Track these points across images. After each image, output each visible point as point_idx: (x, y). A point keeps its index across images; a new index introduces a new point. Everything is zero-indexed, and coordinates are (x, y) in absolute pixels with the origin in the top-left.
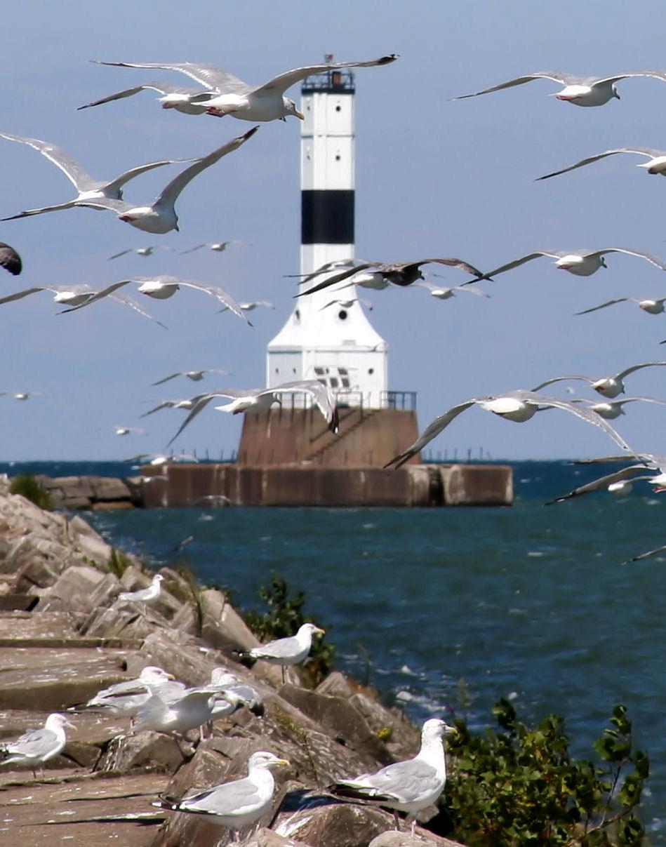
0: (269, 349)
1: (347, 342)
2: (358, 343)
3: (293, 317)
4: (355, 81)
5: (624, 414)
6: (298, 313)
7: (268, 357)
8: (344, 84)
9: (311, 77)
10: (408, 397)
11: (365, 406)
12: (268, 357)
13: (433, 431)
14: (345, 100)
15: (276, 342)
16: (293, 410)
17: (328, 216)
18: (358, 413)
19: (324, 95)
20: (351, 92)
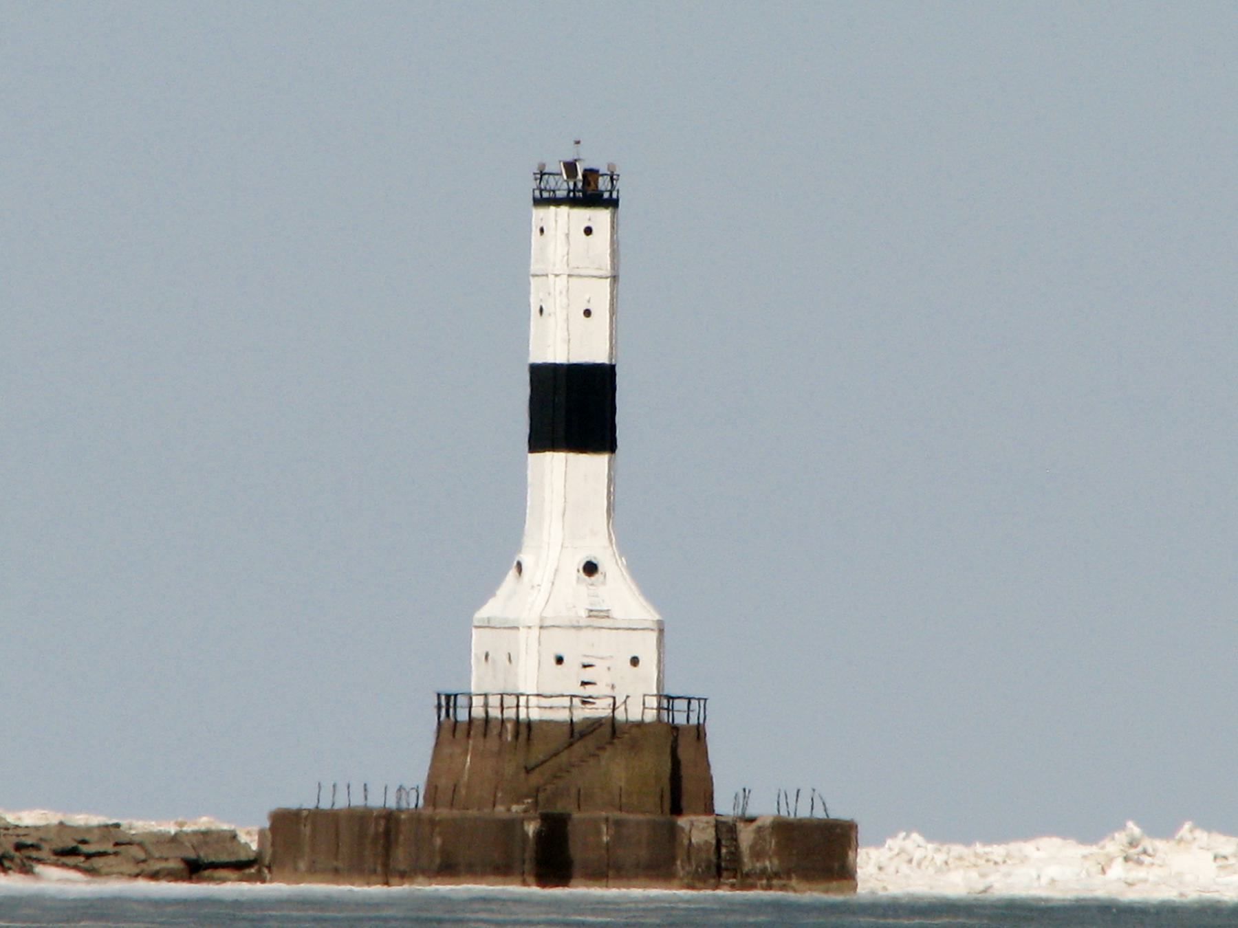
0: (476, 624)
1: (592, 613)
2: (616, 613)
3: (513, 572)
4: (618, 185)
5: (448, 702)
6: (519, 565)
7: (474, 630)
8: (907, 836)
9: (915, 836)
10: (702, 702)
11: (620, 715)
12: (474, 630)
13: (369, 905)
14: (600, 218)
15: (482, 614)
16: (517, 722)
17: (574, 408)
18: (607, 730)
19: (564, 210)
20: (613, 203)
